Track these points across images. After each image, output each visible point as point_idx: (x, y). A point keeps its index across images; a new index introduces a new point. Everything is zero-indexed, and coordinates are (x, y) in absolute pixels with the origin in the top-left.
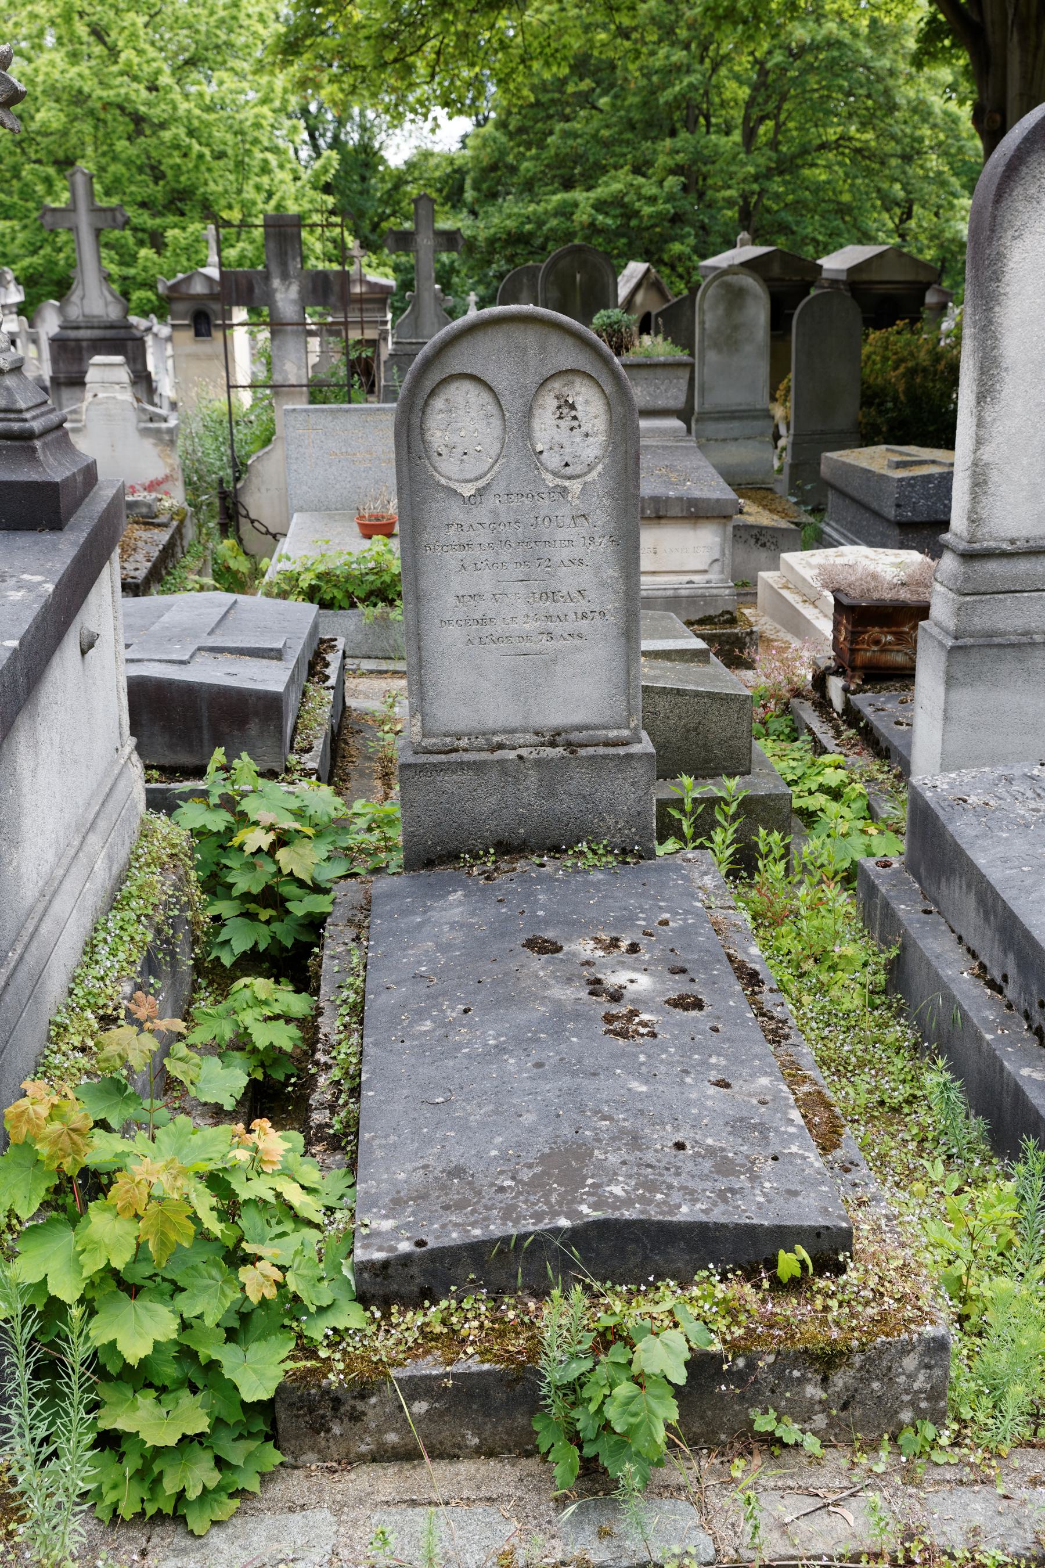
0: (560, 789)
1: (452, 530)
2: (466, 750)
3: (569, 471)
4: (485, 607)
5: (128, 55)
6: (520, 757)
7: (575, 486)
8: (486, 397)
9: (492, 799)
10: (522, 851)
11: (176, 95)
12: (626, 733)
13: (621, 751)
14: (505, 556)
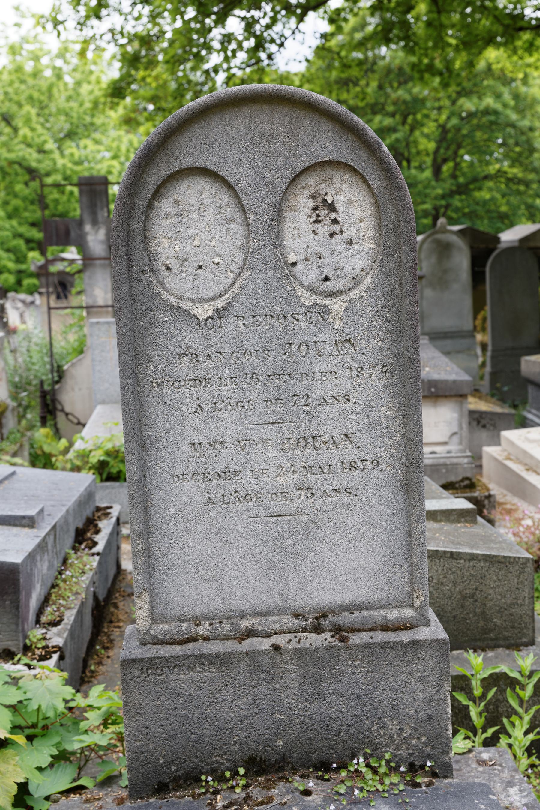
0: (327, 688)
1: (185, 360)
2: (206, 639)
3: (329, 286)
4: (226, 458)
5: (24, 131)
6: (276, 647)
7: (338, 305)
8: (225, 197)
9: (241, 703)
10: (281, 769)
11: (56, 155)
12: (409, 613)
13: (405, 637)
14: (251, 393)
